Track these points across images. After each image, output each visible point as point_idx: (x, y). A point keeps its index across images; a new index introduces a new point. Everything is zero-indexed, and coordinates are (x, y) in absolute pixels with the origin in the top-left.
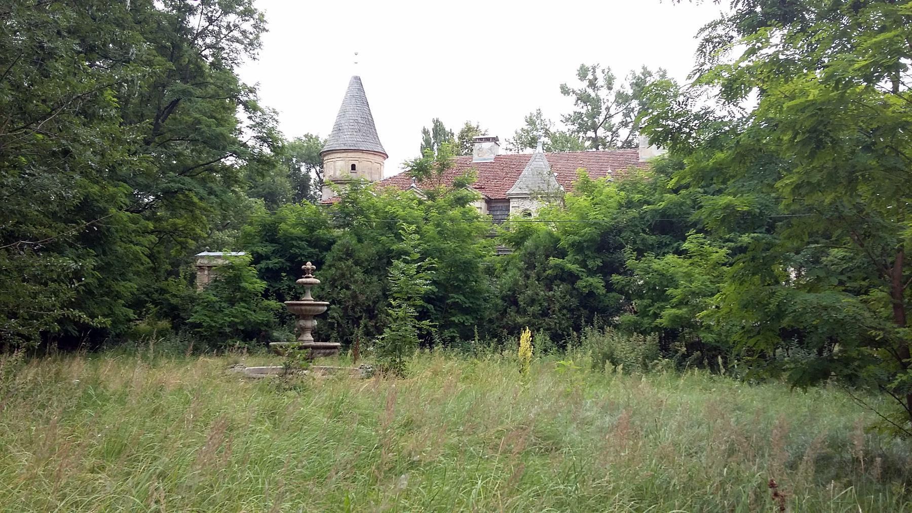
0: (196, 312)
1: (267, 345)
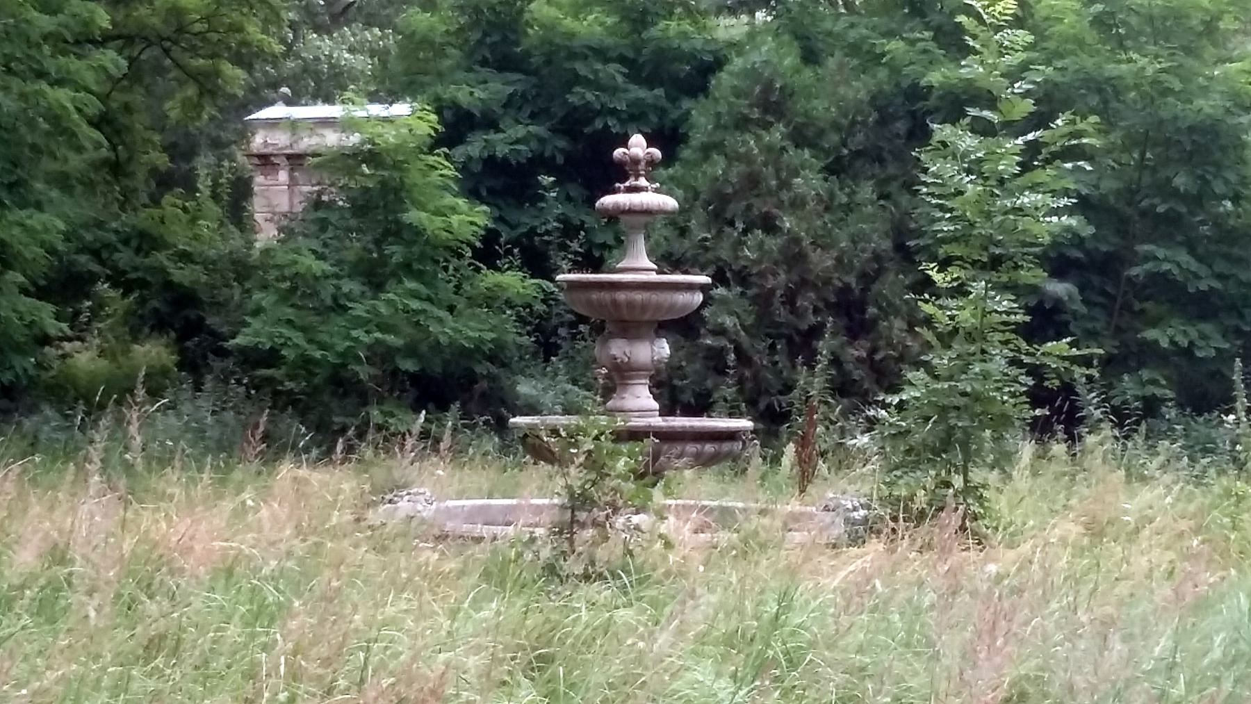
0: (257, 312)
1: (500, 426)
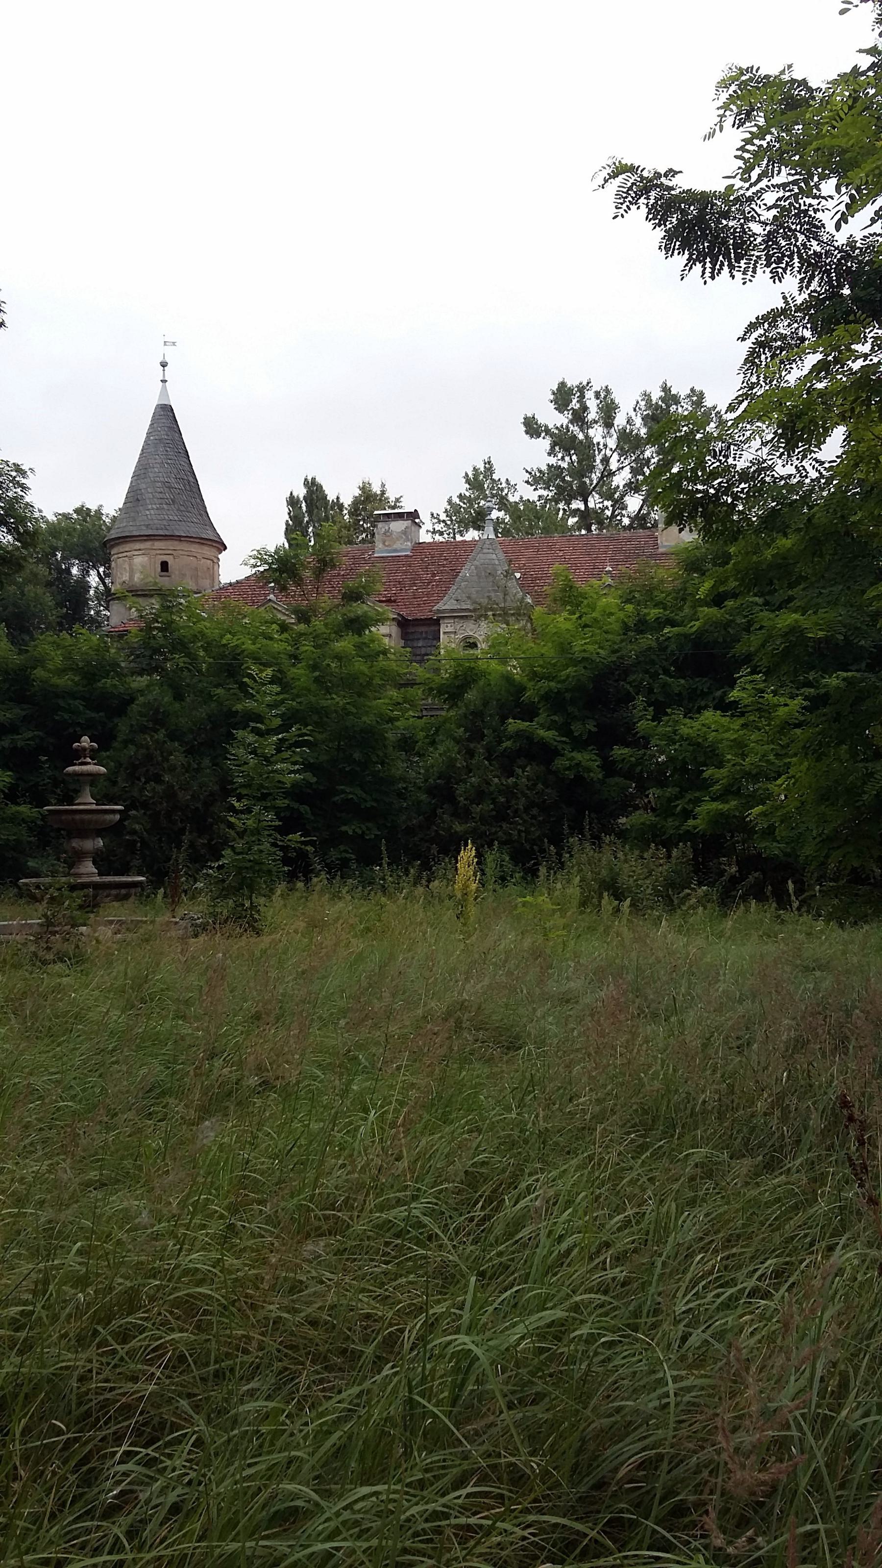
1: (15, 884)
